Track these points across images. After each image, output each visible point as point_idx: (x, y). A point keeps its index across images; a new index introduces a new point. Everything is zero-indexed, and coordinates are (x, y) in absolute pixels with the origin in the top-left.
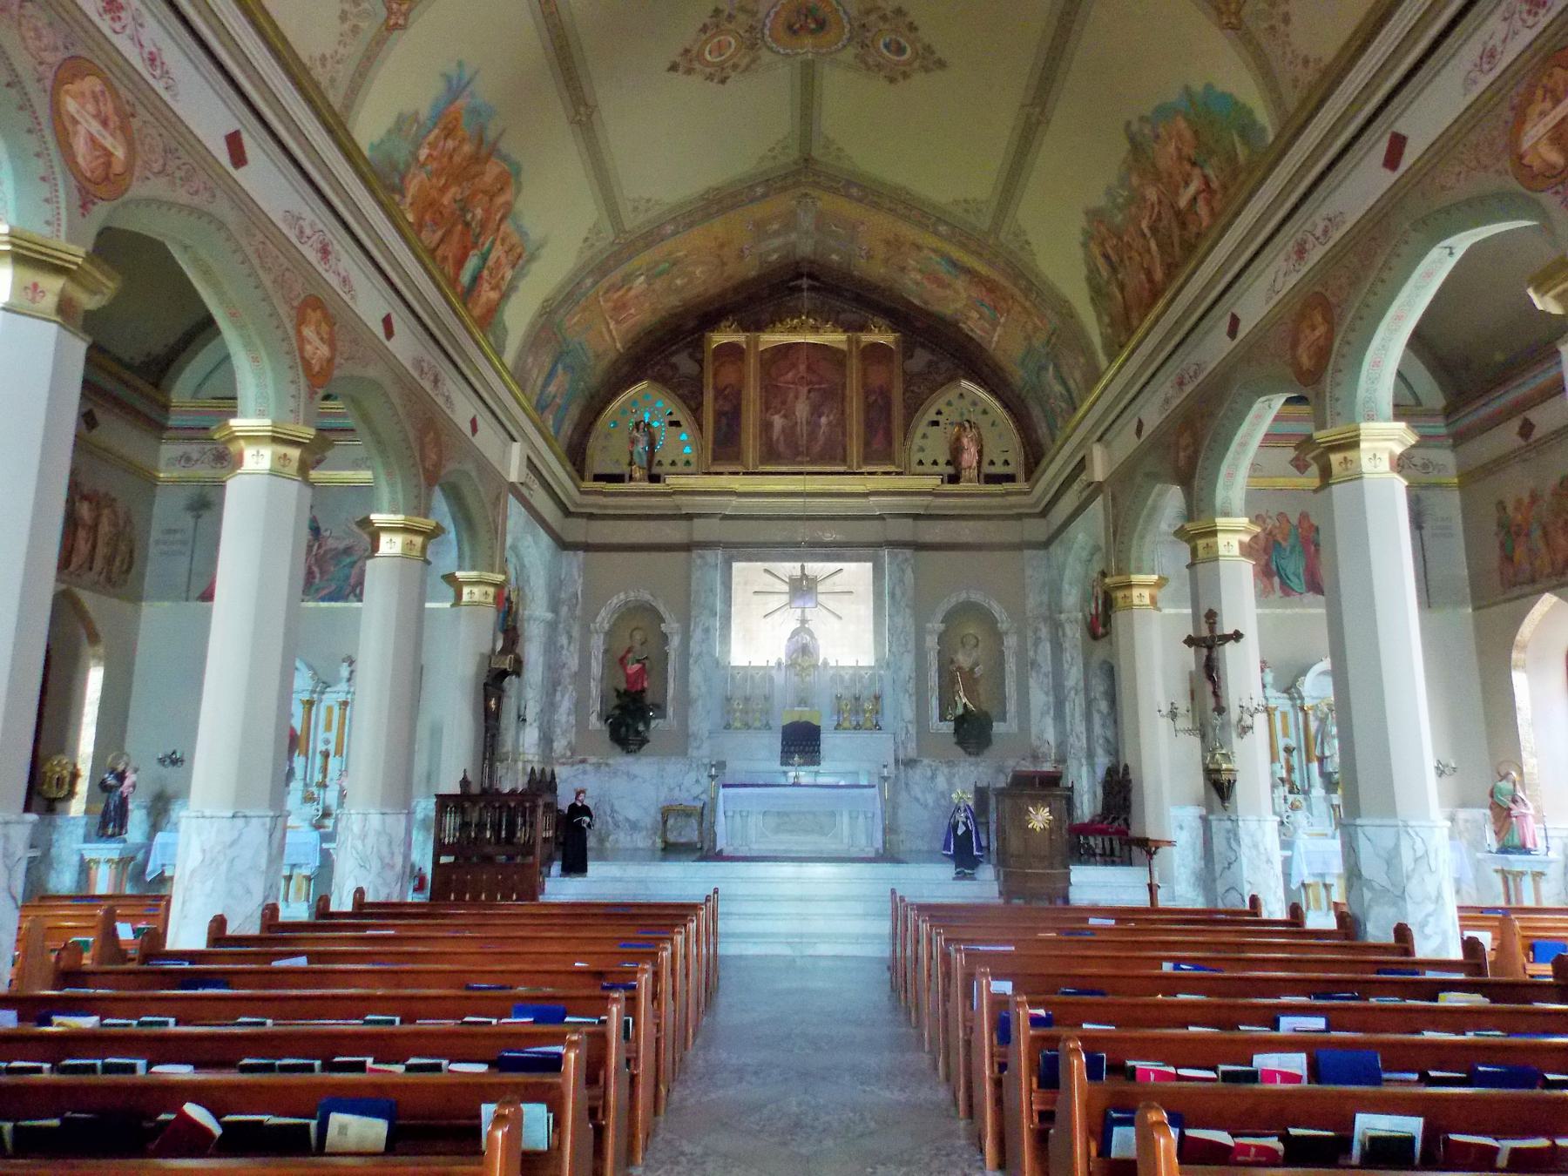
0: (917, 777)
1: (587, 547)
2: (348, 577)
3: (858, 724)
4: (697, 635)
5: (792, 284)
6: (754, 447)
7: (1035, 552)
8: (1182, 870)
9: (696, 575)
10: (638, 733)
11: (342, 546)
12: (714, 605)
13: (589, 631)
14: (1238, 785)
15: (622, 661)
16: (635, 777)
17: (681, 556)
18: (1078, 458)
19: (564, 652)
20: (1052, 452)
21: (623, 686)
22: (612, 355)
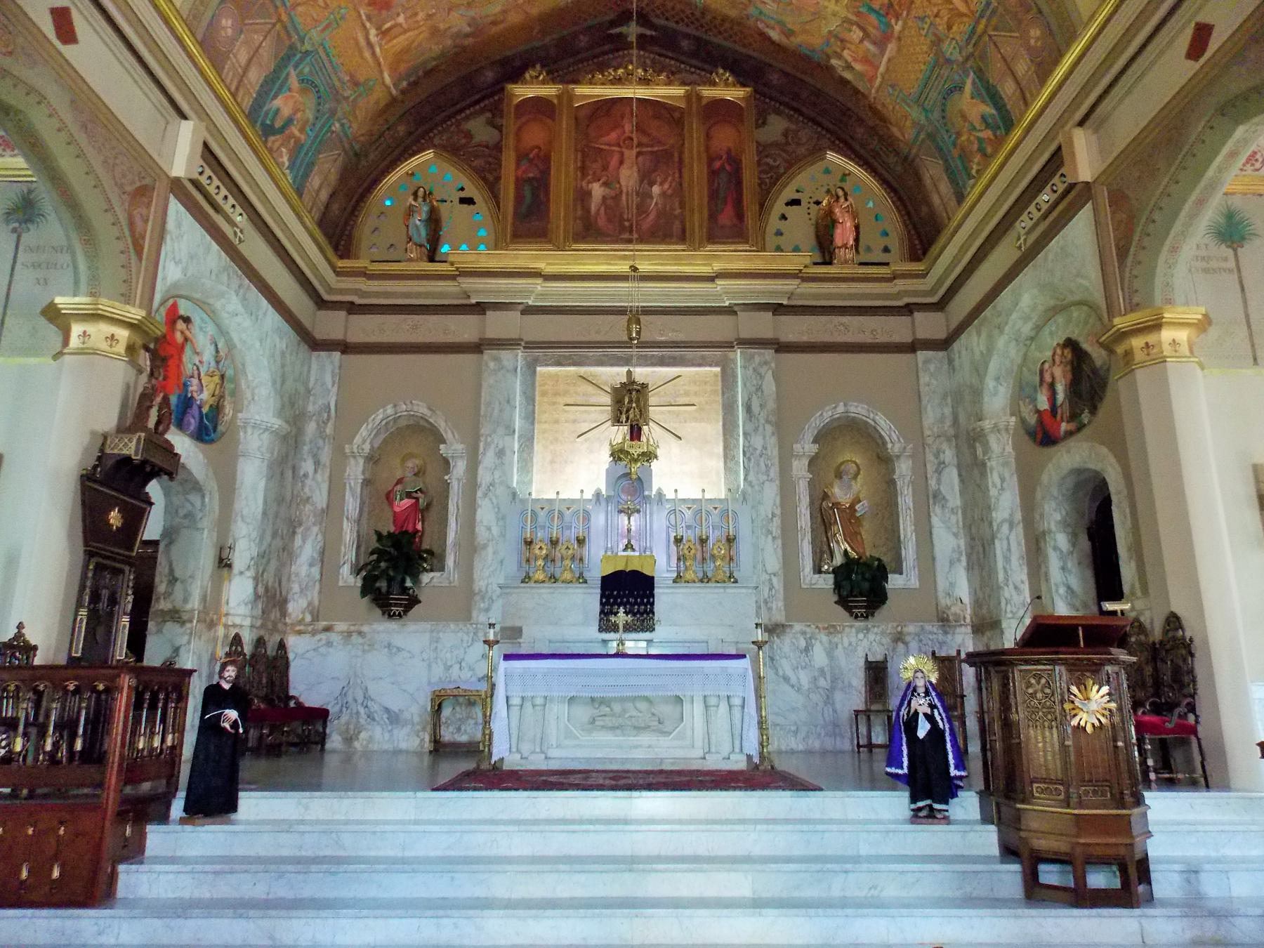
0: (786, 649)
1: (346, 348)
3: (705, 574)
4: (488, 459)
5: (617, 30)
9: (488, 381)
10: (404, 590)
12: (512, 419)
13: (345, 456)
15: (389, 497)
16: (399, 649)
18: (1053, 147)
19: (309, 482)
20: (954, 224)
21: (388, 527)
22: (378, 97)
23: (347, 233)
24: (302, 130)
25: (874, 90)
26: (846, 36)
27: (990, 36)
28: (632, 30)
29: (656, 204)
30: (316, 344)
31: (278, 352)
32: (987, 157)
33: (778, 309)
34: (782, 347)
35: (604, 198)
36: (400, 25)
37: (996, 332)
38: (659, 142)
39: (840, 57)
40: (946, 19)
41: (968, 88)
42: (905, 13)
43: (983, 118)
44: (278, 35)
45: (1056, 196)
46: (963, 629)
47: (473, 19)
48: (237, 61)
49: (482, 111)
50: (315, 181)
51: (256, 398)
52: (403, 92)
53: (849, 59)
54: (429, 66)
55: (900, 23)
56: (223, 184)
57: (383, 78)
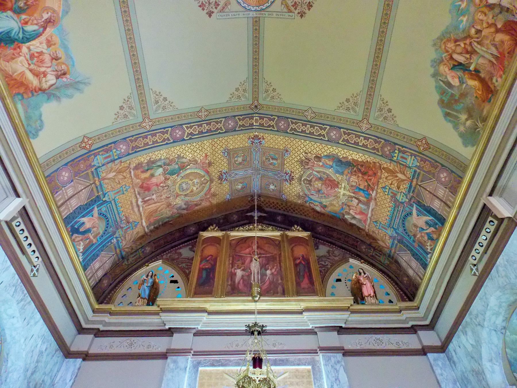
5: (249, 214)
9: (168, 375)
17: (158, 363)
23: (109, 297)
24: (95, 237)
25: (368, 226)
26: (350, 204)
27: (420, 185)
28: (256, 215)
29: (269, 278)
30: (68, 354)
31: (37, 351)
32: (434, 241)
33: (340, 330)
34: (346, 353)
35: (243, 276)
36: (154, 199)
37: (479, 328)
38: (270, 253)
39: (349, 214)
40: (396, 185)
41: (414, 212)
42: (376, 187)
43: (427, 223)
44: (92, 190)
45: (490, 234)
47: (187, 202)
48: (66, 193)
49: (188, 245)
50: (96, 265)
51: (8, 380)
52: (151, 231)
53: (353, 214)
54: (165, 221)
55: (375, 192)
56: (38, 250)
57: (142, 222)
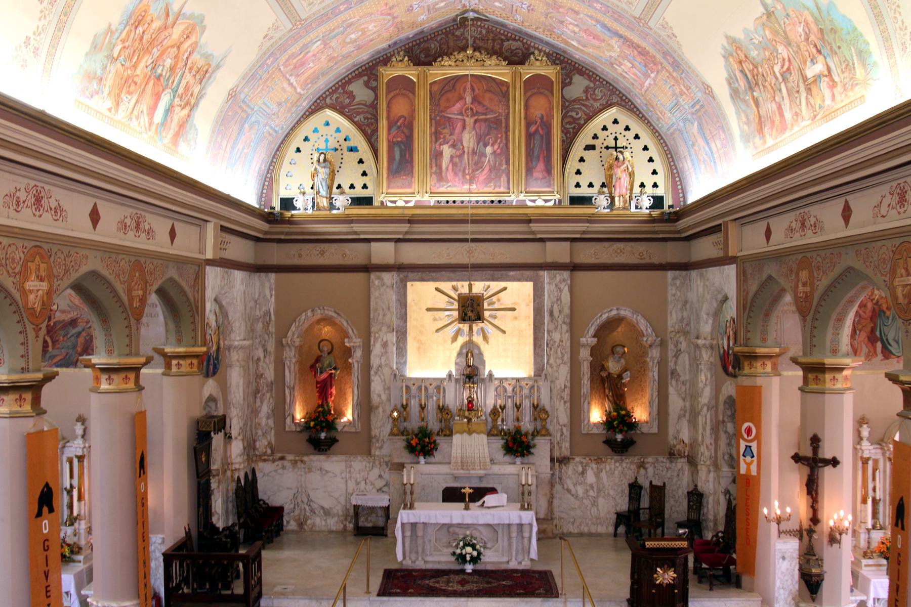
0: (570, 472)
2: (74, 347)
6: (425, 108)
7: (677, 272)
8: (782, 591)
9: (375, 294)
11: (67, 317)
14: (824, 583)
16: (327, 472)
17: (360, 276)
29: (489, 161)
46: (683, 460)
